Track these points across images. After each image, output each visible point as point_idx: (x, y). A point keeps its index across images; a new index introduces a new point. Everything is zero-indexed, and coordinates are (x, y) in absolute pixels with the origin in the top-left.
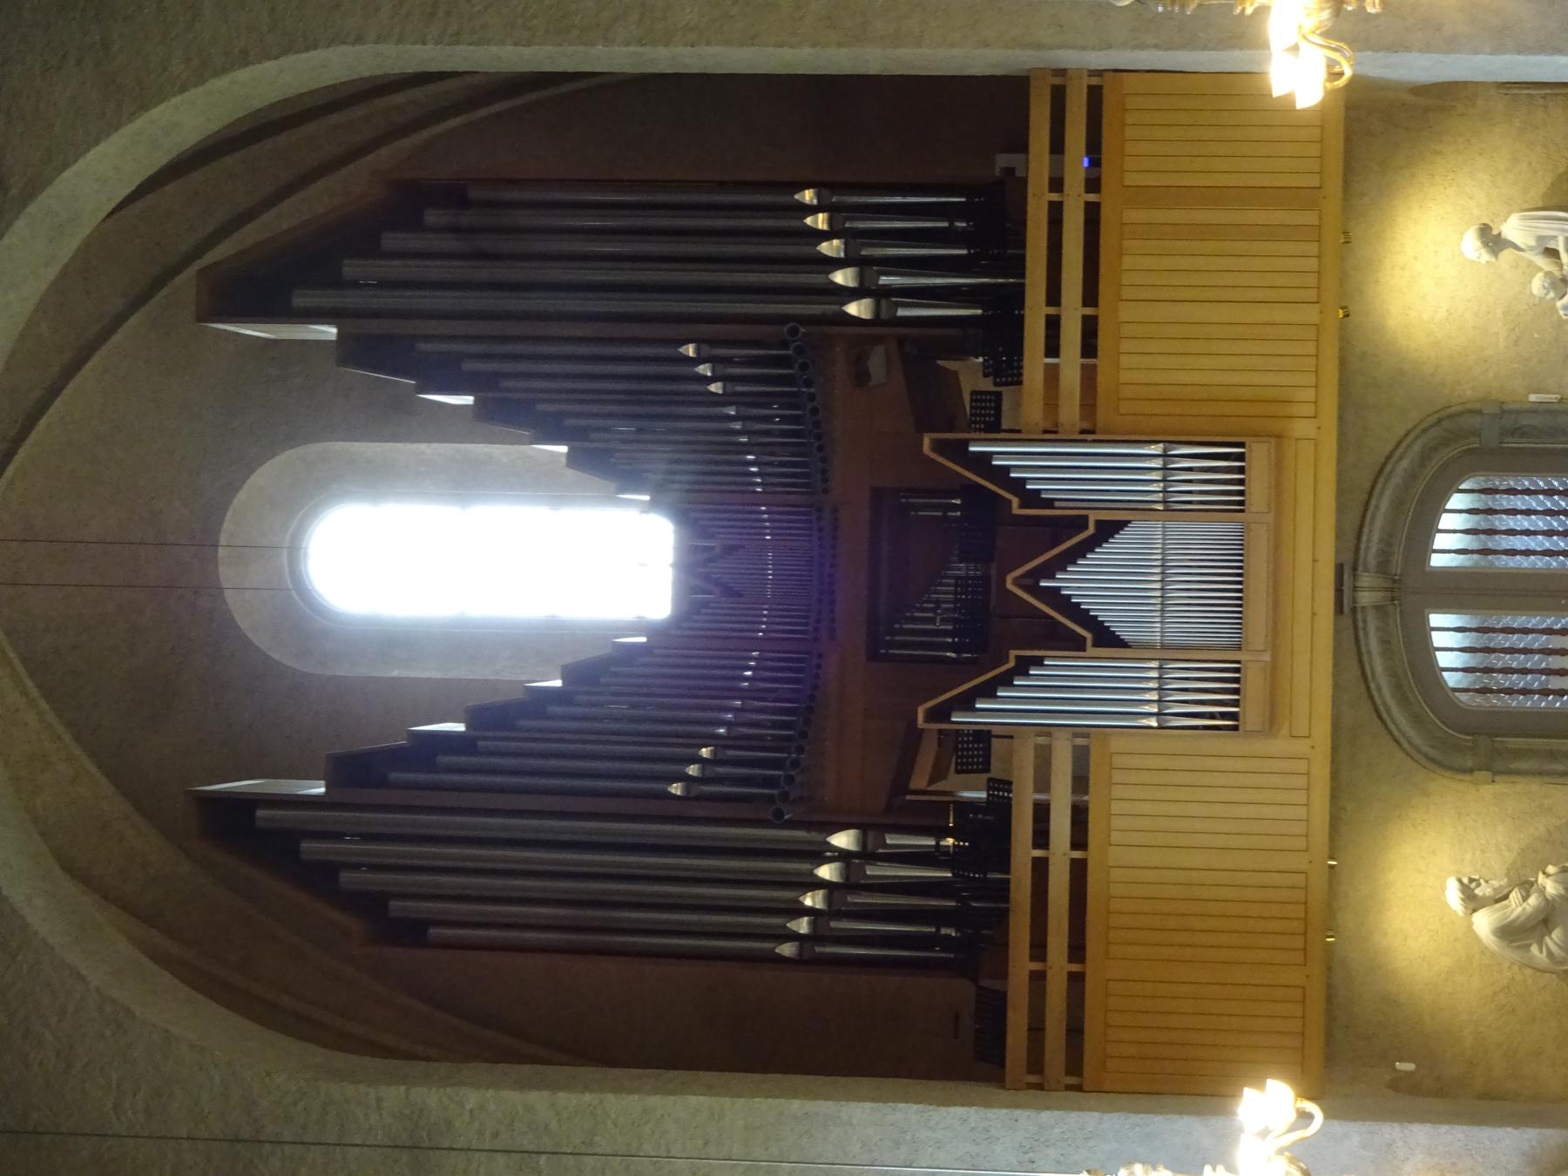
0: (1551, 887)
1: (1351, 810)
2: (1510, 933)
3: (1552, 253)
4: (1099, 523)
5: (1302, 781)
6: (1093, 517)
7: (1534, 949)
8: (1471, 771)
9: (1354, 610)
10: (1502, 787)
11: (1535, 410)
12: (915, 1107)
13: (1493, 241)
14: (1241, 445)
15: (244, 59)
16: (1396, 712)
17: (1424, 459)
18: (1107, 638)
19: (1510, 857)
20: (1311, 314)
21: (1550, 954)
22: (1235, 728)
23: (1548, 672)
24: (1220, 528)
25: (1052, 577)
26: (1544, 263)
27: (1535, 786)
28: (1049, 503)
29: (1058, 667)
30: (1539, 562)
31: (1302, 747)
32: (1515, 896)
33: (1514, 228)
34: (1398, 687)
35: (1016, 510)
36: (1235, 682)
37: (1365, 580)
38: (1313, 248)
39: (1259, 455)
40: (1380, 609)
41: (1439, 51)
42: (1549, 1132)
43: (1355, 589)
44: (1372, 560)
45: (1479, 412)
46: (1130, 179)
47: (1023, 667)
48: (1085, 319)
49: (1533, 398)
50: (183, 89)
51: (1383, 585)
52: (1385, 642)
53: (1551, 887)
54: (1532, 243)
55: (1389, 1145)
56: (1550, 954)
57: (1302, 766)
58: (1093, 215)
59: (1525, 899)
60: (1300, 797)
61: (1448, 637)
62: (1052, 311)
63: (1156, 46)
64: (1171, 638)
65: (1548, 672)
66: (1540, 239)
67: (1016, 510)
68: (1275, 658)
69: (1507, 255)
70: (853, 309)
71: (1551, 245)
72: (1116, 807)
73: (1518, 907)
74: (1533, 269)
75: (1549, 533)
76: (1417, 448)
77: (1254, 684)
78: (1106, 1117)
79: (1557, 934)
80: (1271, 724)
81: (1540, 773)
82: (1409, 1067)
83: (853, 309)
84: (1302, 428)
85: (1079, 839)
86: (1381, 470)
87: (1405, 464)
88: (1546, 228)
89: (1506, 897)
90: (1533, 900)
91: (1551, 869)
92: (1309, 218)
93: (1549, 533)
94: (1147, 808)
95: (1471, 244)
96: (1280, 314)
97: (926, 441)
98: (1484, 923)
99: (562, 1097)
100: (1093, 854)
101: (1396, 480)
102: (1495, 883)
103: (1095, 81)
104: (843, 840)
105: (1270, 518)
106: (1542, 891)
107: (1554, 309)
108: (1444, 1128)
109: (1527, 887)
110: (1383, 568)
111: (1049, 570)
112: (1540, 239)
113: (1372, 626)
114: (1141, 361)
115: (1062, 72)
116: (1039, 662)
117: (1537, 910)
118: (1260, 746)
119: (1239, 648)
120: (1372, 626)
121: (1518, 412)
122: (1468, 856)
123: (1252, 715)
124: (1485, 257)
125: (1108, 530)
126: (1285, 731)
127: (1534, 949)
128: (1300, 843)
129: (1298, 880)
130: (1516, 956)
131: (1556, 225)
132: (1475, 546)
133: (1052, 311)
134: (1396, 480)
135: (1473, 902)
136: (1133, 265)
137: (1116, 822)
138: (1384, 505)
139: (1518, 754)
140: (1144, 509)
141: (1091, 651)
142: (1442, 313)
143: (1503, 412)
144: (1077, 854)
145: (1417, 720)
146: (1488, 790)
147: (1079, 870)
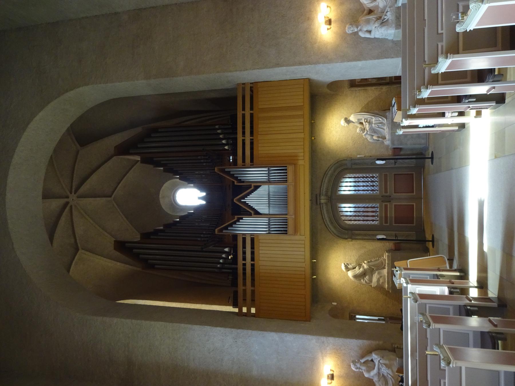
0: (366, 266)
1: (316, 250)
2: (355, 276)
3: (361, 123)
4: (255, 186)
5: (303, 246)
6: (253, 185)
7: (362, 280)
8: (347, 239)
9: (320, 204)
10: (354, 242)
11: (359, 159)
12: (209, 327)
13: (348, 121)
14: (286, 167)
15: (67, 91)
16: (330, 226)
17: (334, 171)
18: (257, 213)
19: (356, 258)
20: (302, 135)
21: (366, 282)
22: (287, 233)
23: (364, 216)
24: (282, 186)
25: (244, 199)
26: (359, 126)
27: (361, 242)
28: (243, 182)
29: (247, 220)
30: (365, 192)
31: (303, 238)
32: (357, 268)
33: (352, 118)
34: (330, 220)
35: (236, 184)
36: (285, 222)
37: (322, 197)
38: (302, 120)
39: (290, 169)
40: (326, 204)
41: (327, 63)
42: (365, 341)
43: (320, 199)
44: (324, 193)
45: (346, 160)
46: (260, 107)
47: (238, 220)
48: (251, 139)
49: (358, 156)
50: (56, 98)
51: (326, 198)
52: (327, 211)
53: (366, 266)
54: (357, 121)
55: (323, 342)
56: (366, 282)
57: (303, 242)
58: (252, 116)
59: (359, 269)
60: (303, 249)
61: (347, 209)
62: (243, 138)
63: (258, 69)
64: (271, 212)
65: (364, 216)
66: (358, 120)
67: (236, 184)
68: (295, 217)
69: (351, 124)
70: (226, 147)
71: (361, 121)
72: (261, 252)
73: (358, 271)
74: (357, 127)
75: (363, 186)
76: (333, 168)
77: (291, 223)
78: (253, 332)
79: (367, 277)
80: (296, 231)
81: (362, 239)
82: (335, 304)
83: (226, 147)
84: (301, 162)
85: (253, 259)
86: (325, 174)
87: (330, 172)
88: (360, 117)
89: (355, 268)
90: (361, 269)
91: (365, 262)
92: (300, 113)
93: (363, 186)
94: (268, 252)
95: (343, 122)
96: (294, 136)
97: (216, 169)
98: (350, 274)
99: (133, 320)
100: (255, 262)
101: (329, 175)
102: (353, 265)
103: (251, 85)
104: (227, 250)
105: (293, 184)
106: (363, 267)
107: (362, 136)
108: (337, 339)
109: (360, 266)
110: (326, 195)
111: (243, 198)
112: (358, 120)
113: (324, 207)
114: (263, 149)
115: (244, 84)
116: (242, 219)
117: (362, 272)
118: (293, 237)
119: (287, 214)
120: (324, 207)
121: (355, 160)
122: (347, 257)
123: (290, 230)
124: (346, 125)
125: (257, 187)
126: (299, 234)
127: (362, 280)
128: (303, 260)
129: (303, 269)
130: (358, 282)
131: (362, 116)
132: (354, 189)
133: (243, 138)
134: (329, 175)
135: (348, 269)
136: (261, 126)
137: (261, 255)
138: (326, 181)
139: (359, 235)
140: (264, 183)
141: (253, 216)
142: (337, 139)
143: (352, 160)
144: (252, 262)
145: (335, 227)
146: (351, 243)
147: (253, 265)
